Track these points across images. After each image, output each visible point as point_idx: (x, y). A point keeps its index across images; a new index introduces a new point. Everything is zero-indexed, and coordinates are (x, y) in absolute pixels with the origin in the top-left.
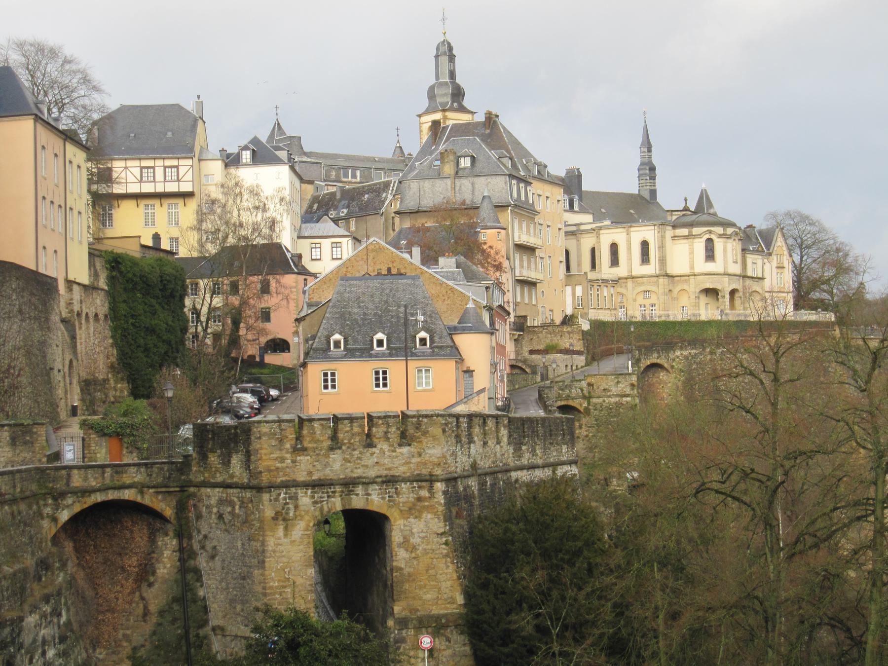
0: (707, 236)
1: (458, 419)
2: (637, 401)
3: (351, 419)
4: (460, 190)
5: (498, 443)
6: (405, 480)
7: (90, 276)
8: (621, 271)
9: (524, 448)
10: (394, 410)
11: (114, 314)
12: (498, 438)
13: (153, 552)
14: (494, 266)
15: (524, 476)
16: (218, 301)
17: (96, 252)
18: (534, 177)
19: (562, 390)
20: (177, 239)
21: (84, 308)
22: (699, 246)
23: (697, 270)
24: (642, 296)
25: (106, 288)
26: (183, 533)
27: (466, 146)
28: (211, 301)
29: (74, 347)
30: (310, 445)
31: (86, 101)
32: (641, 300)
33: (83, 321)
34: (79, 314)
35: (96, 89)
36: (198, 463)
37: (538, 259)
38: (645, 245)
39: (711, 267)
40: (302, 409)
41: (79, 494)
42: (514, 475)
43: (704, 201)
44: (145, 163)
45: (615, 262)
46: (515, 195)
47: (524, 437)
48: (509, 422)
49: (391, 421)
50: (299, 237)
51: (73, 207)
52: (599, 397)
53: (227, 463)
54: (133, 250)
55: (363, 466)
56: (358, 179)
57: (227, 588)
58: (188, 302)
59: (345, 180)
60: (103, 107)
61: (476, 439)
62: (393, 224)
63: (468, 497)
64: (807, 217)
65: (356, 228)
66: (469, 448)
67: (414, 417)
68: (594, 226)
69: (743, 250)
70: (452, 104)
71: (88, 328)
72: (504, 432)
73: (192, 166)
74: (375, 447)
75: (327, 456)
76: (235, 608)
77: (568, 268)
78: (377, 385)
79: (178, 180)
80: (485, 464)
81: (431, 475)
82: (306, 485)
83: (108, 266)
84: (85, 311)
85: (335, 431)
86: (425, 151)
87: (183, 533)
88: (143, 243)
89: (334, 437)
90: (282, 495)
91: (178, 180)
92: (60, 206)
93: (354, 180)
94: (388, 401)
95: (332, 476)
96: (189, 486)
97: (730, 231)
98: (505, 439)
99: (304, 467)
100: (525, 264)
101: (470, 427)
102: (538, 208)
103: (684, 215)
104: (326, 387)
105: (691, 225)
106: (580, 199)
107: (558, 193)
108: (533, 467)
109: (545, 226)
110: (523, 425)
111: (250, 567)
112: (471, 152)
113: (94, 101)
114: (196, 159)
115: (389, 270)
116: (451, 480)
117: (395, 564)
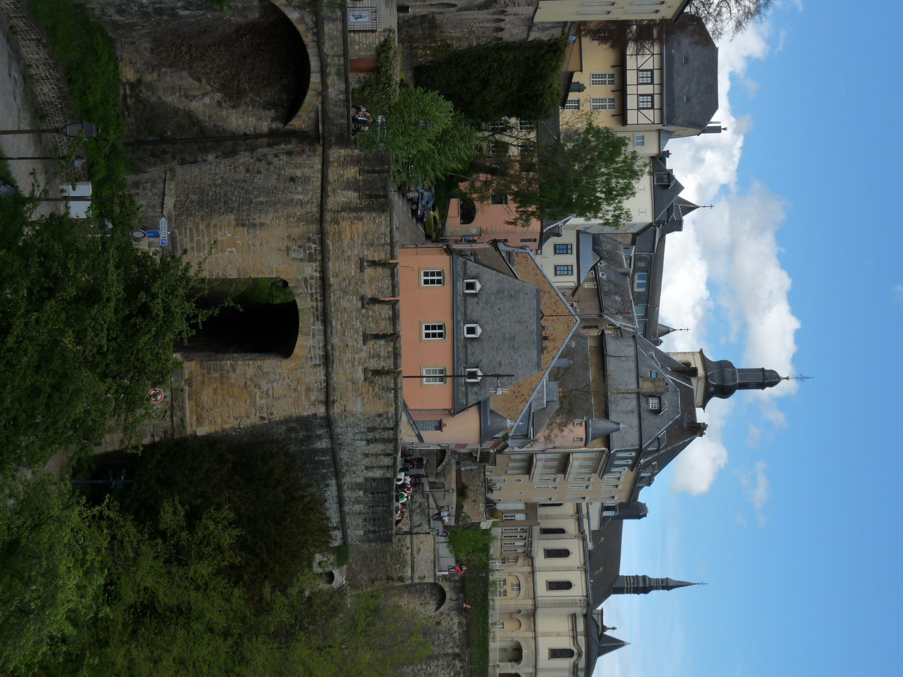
0: (575, 651)
1: (392, 429)
2: (409, 582)
4: (626, 398)
5: (367, 468)
6: (328, 375)
7: (542, 23)
8: (540, 560)
9: (361, 493)
10: (402, 365)
11: (502, 47)
12: (372, 467)
13: (253, 106)
14: (549, 436)
15: (331, 492)
16: (514, 151)
17: (567, 30)
18: (638, 473)
19: (420, 506)
20: (578, 108)
21: (510, 17)
22: (565, 643)
23: (540, 640)
24: (515, 582)
25: (530, 39)
26: (274, 137)
27: (671, 403)
28: (514, 146)
29: (468, 8)
30: (366, 276)
31: (726, 15)
32: (511, 580)
33: (496, 17)
35: (739, 25)
36: (349, 155)
37: (554, 476)
38: (567, 585)
39: (544, 654)
40: (403, 246)
41: (315, 30)
42: (333, 482)
44: (656, 74)
46: (620, 455)
47: (372, 493)
48: (389, 479)
50: (578, 232)
51: (615, 6)
52: (412, 543)
53: (353, 185)
54: (569, 64)
55: (344, 330)
56: (636, 290)
57: (215, 186)
58: (513, 121)
59: (636, 277)
60: (720, 34)
61: (371, 446)
62: (591, 327)
63: (309, 438)
65: (587, 289)
66: (362, 440)
67: (396, 384)
68: (587, 532)
70: (713, 386)
71: (489, 21)
72: (378, 474)
73: (653, 123)
74: (364, 344)
75: (356, 293)
76: (194, 193)
78: (427, 328)
79: (639, 109)
80: (344, 455)
81: (333, 402)
82: (323, 271)
83: (552, 41)
84: (507, 19)
86: (665, 359)
87: (274, 137)
88: (575, 75)
90: (313, 246)
91: (639, 109)
94: (410, 331)
95: (333, 299)
96: (323, 146)
98: (370, 474)
99: (342, 269)
100: (549, 464)
101: (384, 441)
102: (606, 477)
103: (598, 626)
105: (587, 635)
106: (614, 518)
107: (620, 497)
108: (341, 502)
109: (587, 483)
110: (385, 492)
111: (238, 210)
112: (665, 408)
113: (725, 24)
114: (660, 127)
115: (545, 338)
116: (328, 422)
117: (240, 363)
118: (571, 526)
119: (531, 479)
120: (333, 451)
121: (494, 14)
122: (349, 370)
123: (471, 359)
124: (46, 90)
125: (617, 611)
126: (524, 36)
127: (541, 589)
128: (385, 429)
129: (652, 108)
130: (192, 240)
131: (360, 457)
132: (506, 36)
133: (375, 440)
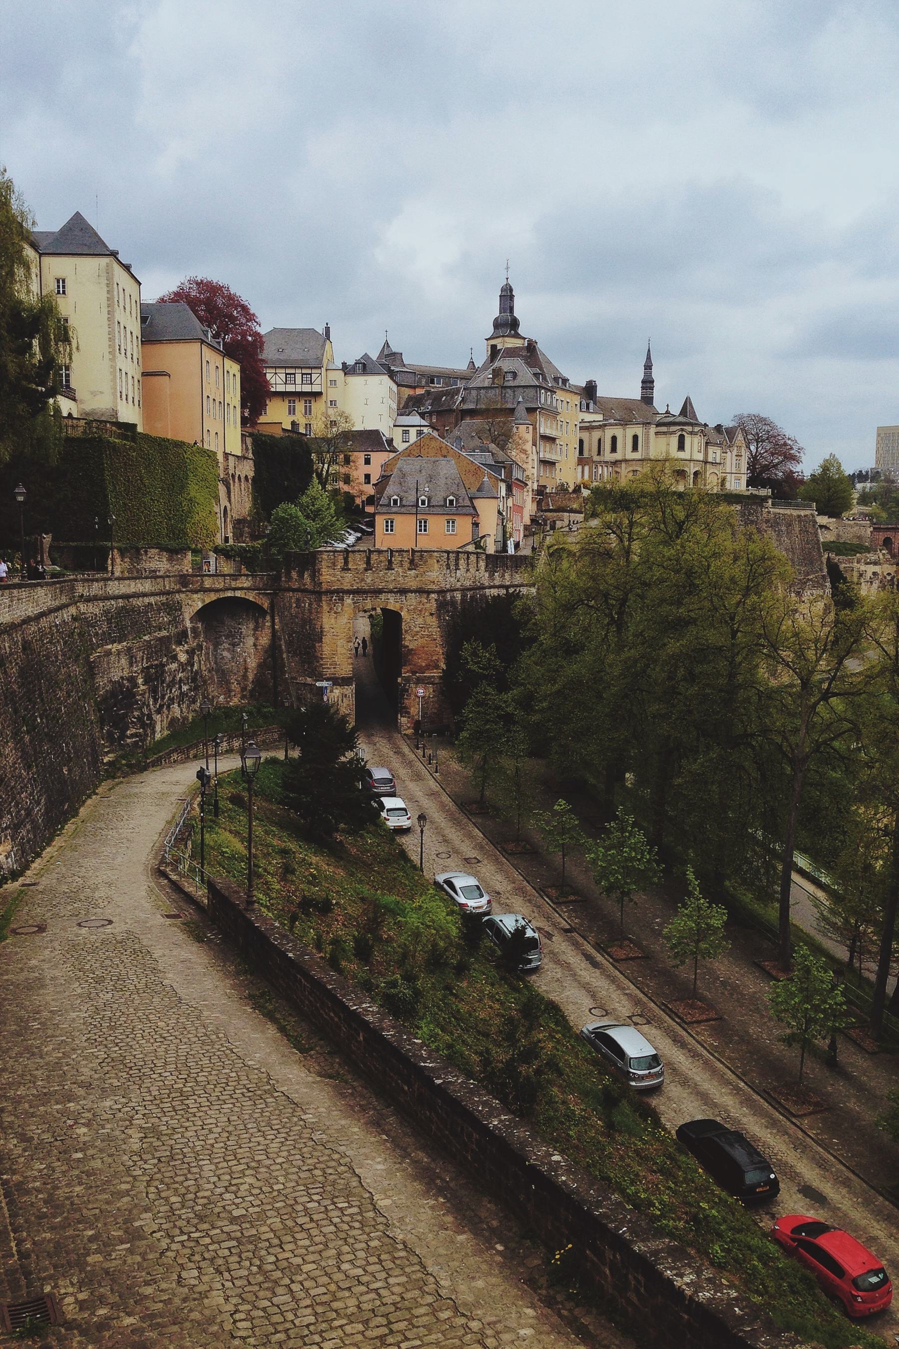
3: (401, 551)
6: (412, 592)
8: (618, 456)
22: (674, 440)
34: (233, 476)
38: (635, 438)
39: (681, 455)
43: (687, 408)
45: (614, 449)
49: (405, 554)
53: (301, 575)
63: (453, 602)
64: (765, 419)
69: (706, 443)
72: (482, 564)
77: (581, 452)
78: (387, 530)
80: (468, 583)
82: (349, 592)
84: (238, 473)
85: (369, 559)
89: (368, 562)
92: (220, 403)
93: (438, 387)
97: (697, 429)
98: (483, 568)
99: (348, 581)
100: (548, 449)
101: (457, 559)
104: (387, 530)
114: (323, 370)
116: (441, 592)
118: (596, 434)
119: (558, 461)
120: (464, 590)
121: (234, 482)
122: (411, 579)
123: (442, 503)
124: (237, 744)
125: (666, 400)
126: (251, 462)
127: (637, 456)
128: (448, 559)
129: (311, 374)
130: (329, 668)
131: (469, 574)
132: (251, 474)
133: (457, 565)
